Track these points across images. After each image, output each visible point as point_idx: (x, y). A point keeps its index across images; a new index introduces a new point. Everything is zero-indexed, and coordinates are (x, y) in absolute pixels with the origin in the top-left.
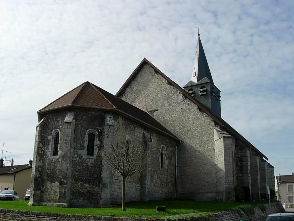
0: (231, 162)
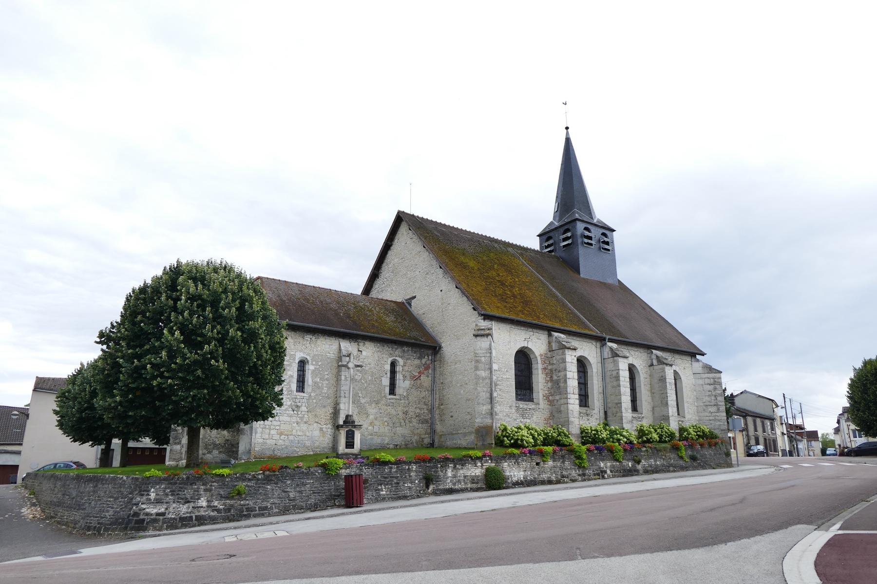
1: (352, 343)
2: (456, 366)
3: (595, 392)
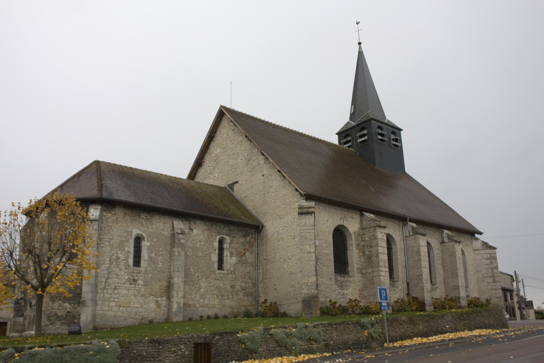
0: (312, 253)
1: (184, 222)
2: (279, 243)
3: (399, 266)
